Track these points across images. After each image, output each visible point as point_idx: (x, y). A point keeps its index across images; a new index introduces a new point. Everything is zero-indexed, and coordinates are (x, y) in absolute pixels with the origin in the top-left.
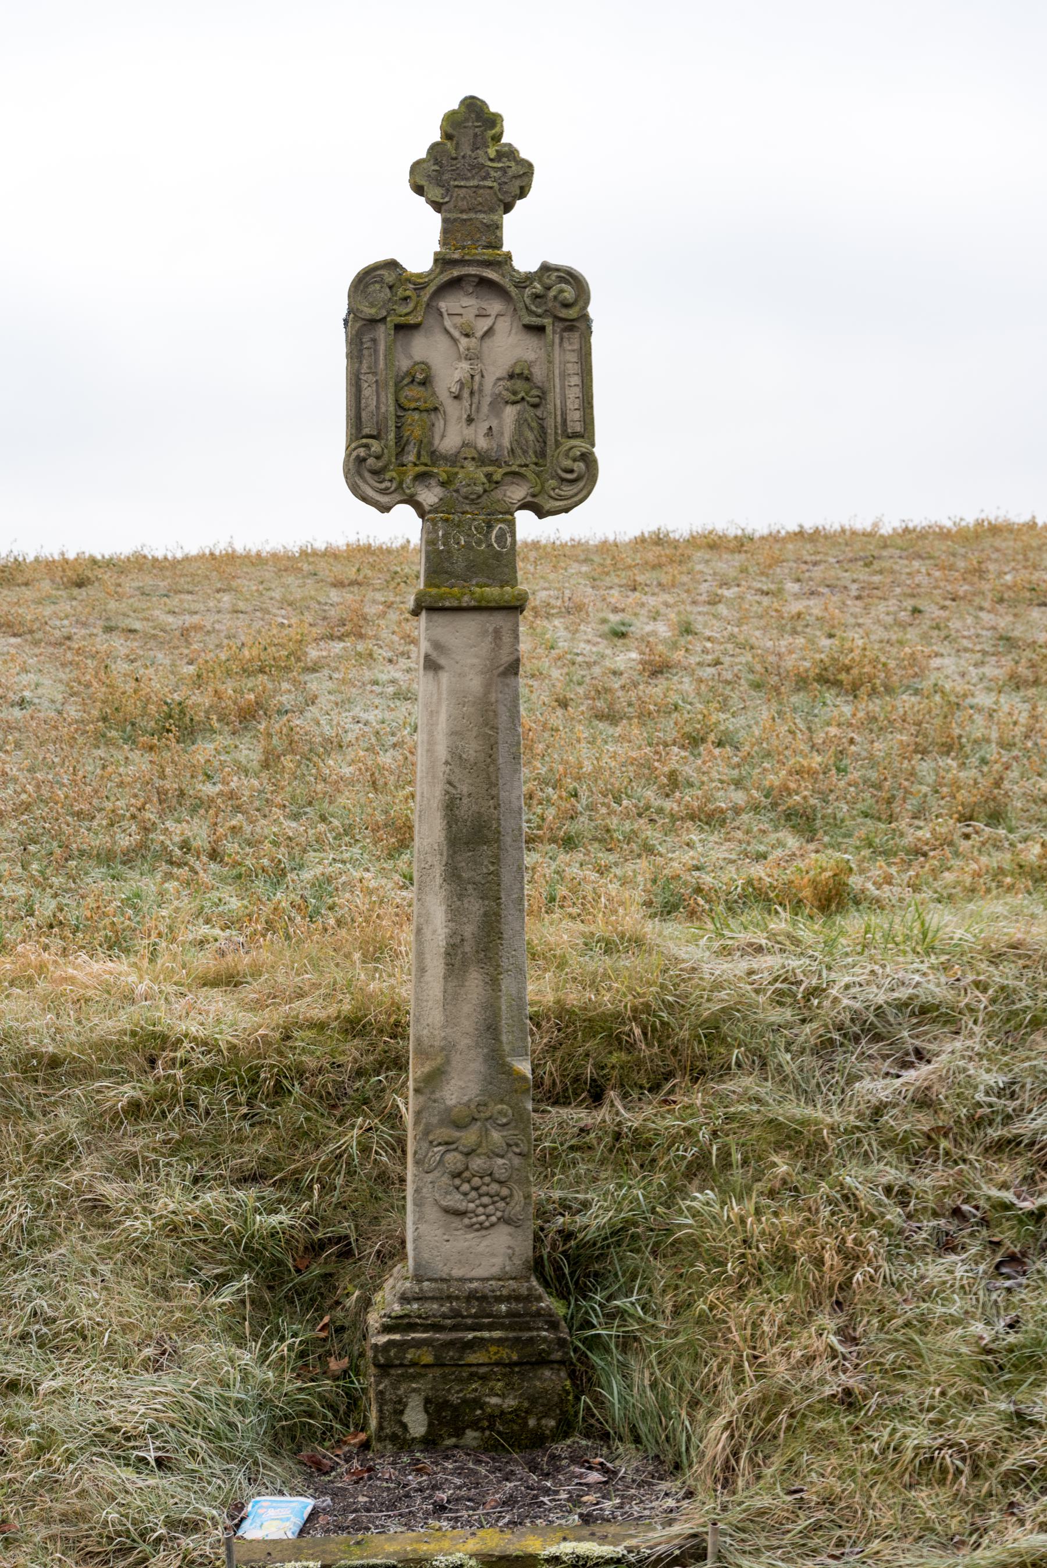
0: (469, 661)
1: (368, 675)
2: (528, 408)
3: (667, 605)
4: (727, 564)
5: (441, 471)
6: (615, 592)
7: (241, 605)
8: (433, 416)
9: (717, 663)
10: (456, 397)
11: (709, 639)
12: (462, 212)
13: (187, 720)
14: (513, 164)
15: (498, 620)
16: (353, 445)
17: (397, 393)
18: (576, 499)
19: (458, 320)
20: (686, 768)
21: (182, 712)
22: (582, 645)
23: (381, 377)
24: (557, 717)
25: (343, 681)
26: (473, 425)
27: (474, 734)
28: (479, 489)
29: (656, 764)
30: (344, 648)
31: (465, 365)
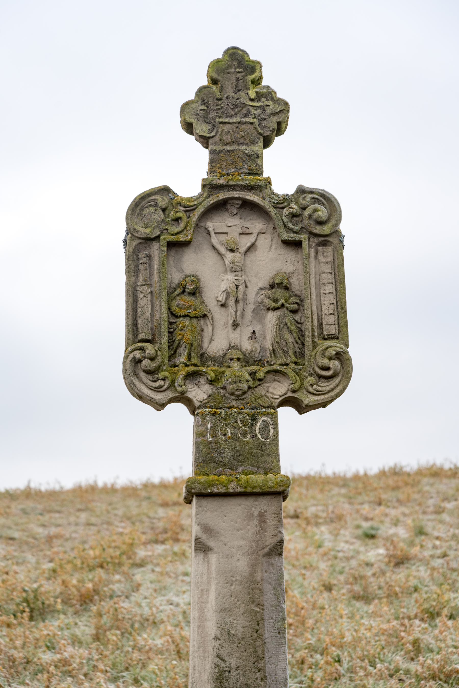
0: (236, 543)
1: (181, 568)
2: (286, 312)
3: (404, 515)
4: (447, 486)
5: (210, 371)
6: (366, 506)
7: (93, 520)
8: (202, 322)
9: (444, 555)
10: (222, 305)
11: (437, 538)
12: (226, 144)
13: (39, 603)
14: (270, 103)
15: (263, 504)
16: (130, 348)
17: (169, 302)
18: (333, 394)
19: (224, 238)
20: (426, 637)
21: (36, 598)
22: (342, 544)
23: (155, 289)
24: (324, 599)
25: (161, 574)
26: (238, 329)
27: (242, 610)
28: (245, 386)
29: (403, 634)
30: (165, 550)
31: (231, 277)
